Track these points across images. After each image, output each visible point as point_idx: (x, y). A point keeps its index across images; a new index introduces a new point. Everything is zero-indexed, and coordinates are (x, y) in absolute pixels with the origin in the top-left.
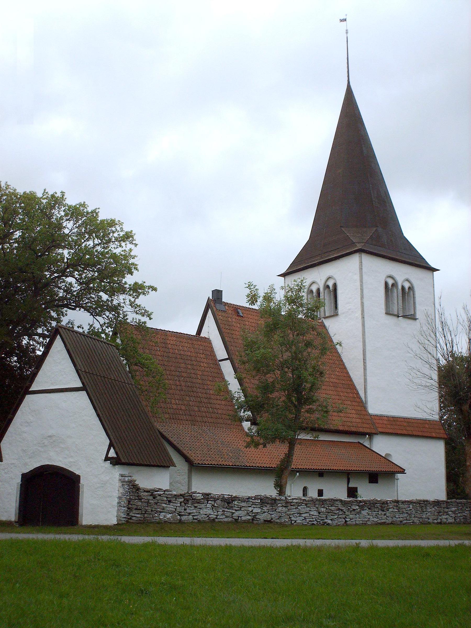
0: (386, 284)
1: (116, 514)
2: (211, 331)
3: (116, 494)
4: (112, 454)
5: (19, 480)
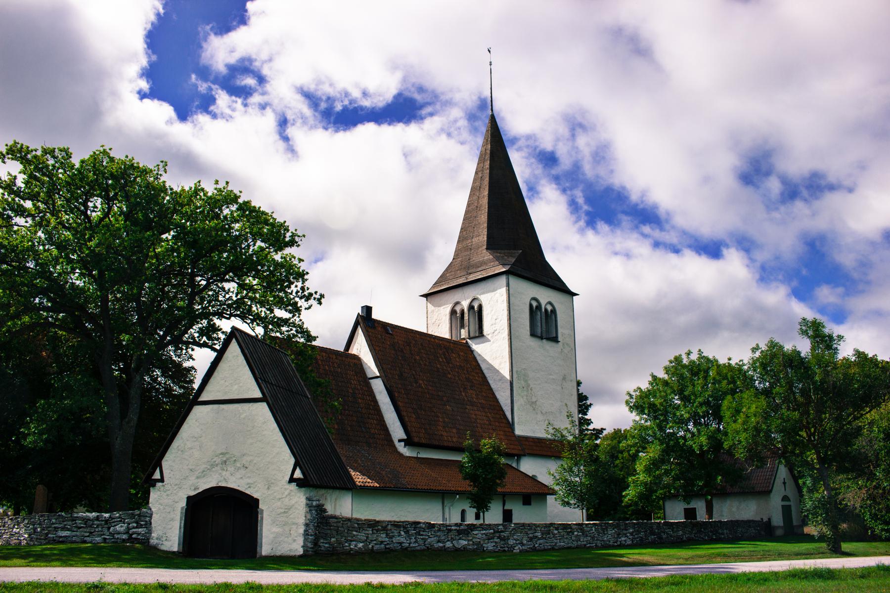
0: (531, 305)
1: (302, 544)
2: (361, 348)
3: (302, 520)
4: (298, 474)
5: (183, 504)
